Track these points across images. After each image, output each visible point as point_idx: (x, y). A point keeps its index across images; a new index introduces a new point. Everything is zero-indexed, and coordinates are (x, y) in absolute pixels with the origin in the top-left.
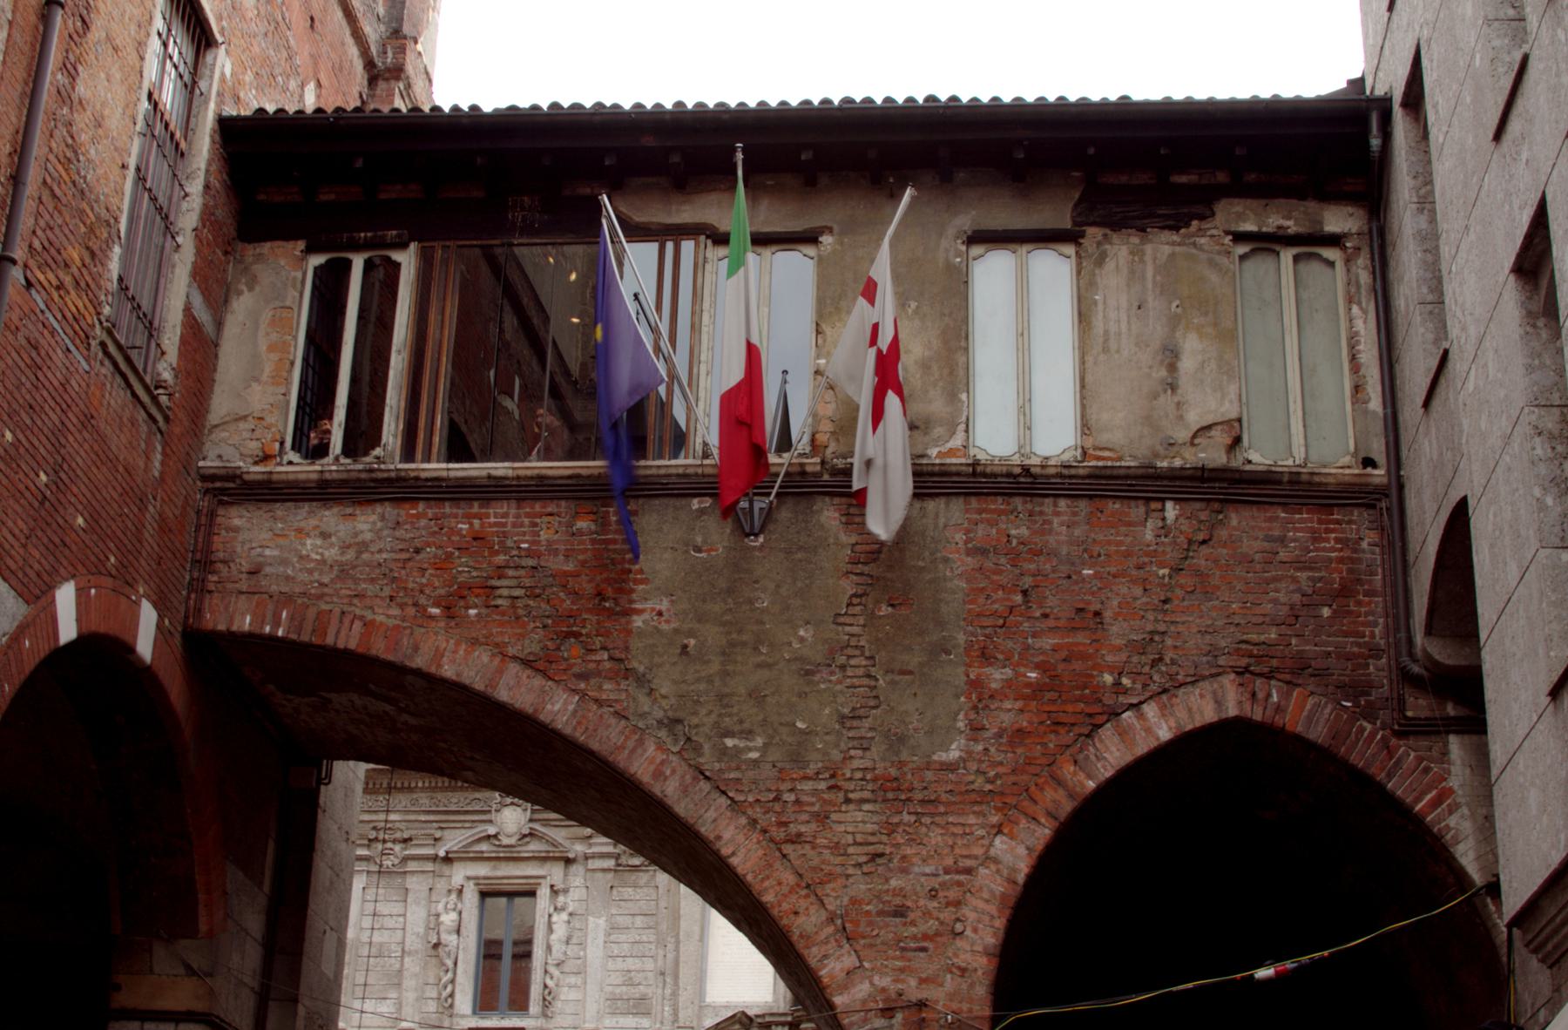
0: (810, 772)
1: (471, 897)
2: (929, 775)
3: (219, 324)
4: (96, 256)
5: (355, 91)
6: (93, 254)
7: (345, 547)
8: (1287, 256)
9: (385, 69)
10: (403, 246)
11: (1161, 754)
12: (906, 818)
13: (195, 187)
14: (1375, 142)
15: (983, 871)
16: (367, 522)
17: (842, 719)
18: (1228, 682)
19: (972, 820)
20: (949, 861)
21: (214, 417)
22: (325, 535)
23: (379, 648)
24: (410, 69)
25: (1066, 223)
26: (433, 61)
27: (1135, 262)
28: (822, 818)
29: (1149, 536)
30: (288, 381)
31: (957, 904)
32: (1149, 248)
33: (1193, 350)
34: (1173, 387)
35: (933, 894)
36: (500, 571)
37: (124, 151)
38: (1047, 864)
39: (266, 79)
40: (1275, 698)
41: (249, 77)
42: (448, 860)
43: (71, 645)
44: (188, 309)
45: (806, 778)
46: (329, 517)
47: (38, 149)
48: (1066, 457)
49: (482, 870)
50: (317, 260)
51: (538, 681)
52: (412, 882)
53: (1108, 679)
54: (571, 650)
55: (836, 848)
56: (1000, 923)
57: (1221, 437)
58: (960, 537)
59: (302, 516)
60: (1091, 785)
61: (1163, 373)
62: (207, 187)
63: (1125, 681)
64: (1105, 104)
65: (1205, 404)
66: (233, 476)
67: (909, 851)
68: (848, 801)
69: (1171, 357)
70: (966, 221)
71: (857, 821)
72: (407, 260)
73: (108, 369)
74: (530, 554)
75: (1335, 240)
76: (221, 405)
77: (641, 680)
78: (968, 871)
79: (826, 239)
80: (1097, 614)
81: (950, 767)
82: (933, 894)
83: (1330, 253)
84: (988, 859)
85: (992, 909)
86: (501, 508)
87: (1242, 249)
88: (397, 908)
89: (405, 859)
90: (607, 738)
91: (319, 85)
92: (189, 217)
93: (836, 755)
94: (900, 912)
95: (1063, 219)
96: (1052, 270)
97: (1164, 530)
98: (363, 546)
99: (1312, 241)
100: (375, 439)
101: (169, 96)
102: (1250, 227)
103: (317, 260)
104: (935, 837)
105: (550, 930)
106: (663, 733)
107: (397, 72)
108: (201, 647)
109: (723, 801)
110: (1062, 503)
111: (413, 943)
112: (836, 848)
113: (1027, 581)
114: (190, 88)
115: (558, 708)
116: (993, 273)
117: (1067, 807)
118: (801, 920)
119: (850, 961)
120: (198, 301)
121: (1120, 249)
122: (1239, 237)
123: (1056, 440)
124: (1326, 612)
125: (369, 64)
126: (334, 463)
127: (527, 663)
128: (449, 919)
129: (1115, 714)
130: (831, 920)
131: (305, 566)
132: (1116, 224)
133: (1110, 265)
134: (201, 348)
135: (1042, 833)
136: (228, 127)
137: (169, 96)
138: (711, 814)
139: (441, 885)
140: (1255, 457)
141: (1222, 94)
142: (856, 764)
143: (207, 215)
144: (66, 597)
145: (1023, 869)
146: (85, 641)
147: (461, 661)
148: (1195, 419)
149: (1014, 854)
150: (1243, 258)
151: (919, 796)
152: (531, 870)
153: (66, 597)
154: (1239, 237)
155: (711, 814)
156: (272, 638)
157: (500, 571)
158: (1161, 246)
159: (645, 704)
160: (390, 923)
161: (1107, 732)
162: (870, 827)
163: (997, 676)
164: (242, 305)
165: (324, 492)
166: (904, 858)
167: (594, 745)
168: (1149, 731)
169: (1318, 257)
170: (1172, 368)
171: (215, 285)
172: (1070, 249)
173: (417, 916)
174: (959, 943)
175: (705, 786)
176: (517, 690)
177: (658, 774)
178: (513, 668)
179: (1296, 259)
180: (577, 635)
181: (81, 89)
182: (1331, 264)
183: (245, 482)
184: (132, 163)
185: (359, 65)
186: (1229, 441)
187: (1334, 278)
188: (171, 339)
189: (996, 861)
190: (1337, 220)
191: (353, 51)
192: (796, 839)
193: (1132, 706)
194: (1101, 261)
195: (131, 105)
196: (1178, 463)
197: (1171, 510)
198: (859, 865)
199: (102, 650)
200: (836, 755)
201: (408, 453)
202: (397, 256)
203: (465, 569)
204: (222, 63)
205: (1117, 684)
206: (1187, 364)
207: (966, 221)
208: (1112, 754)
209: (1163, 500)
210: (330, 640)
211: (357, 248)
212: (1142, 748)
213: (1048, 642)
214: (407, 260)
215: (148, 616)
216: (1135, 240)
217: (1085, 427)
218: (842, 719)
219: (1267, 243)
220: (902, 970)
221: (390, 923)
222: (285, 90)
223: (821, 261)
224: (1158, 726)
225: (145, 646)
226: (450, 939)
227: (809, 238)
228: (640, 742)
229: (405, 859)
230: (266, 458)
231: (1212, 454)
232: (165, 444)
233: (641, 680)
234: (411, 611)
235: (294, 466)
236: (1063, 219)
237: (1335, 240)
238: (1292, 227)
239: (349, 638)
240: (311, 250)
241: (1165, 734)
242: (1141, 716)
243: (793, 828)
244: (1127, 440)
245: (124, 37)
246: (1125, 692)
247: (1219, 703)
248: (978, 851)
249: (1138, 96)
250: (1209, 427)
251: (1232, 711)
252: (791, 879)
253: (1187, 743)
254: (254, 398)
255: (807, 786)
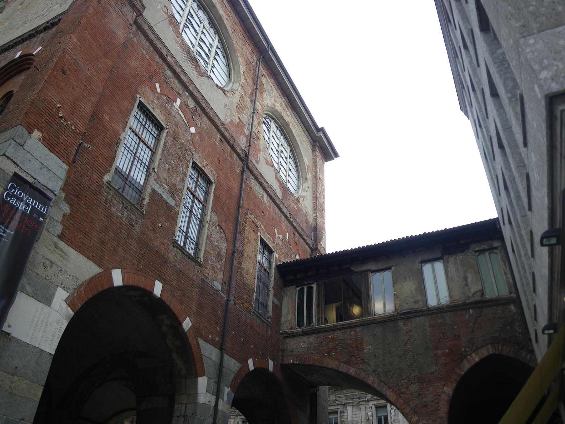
0: (403, 378)
1: (374, 409)
2: (428, 376)
3: (281, 304)
4: (251, 296)
5: (308, 254)
6: (249, 296)
7: (308, 344)
8: (487, 253)
9: (314, 249)
10: (313, 283)
11: (477, 365)
12: (425, 385)
13: (272, 279)
14: (498, 227)
15: (442, 395)
16: (312, 338)
17: (409, 366)
18: (489, 346)
19: (439, 384)
20: (435, 394)
21: (282, 322)
22: (304, 342)
23: (317, 363)
24: (319, 248)
25: (440, 256)
26: (325, 245)
27: (455, 260)
28: (407, 388)
29: (467, 317)
30: (295, 313)
31: (438, 403)
32: (458, 258)
33: (470, 277)
34: (467, 285)
35: (432, 401)
36: (338, 345)
37: (254, 276)
38: (456, 391)
39: (286, 256)
40: (500, 348)
41: (282, 256)
42: (368, 401)
43: (252, 371)
44: (273, 302)
45: (403, 379)
46: (305, 338)
47: (234, 278)
48: (448, 303)
49: (375, 402)
50: (298, 289)
51: (347, 366)
52: (361, 406)
53: (463, 349)
54: (353, 359)
55: (411, 394)
56: (448, 406)
57: (479, 294)
58: (428, 324)
59: (300, 339)
60: (463, 373)
61: (465, 282)
62: (275, 279)
63: (467, 349)
64: (442, 230)
65: (474, 288)
66: (286, 333)
67: (426, 393)
68: (412, 383)
69: (466, 279)
70: (420, 259)
71: (414, 388)
72: (314, 286)
73: (255, 316)
74: (343, 340)
75: (497, 248)
76: (283, 319)
77: (367, 363)
78: (439, 395)
79: (393, 268)
80: (459, 336)
81: (432, 373)
82: (432, 401)
83: (496, 251)
84: (443, 392)
85: (446, 403)
86: (336, 332)
87: (477, 254)
88: (359, 412)
89: (360, 402)
90: (362, 376)
91: (299, 255)
92: (272, 285)
93: (408, 374)
94: (426, 406)
95: (439, 254)
96: (439, 266)
97: (470, 315)
98: (311, 343)
99: (491, 249)
100: (312, 322)
101: (265, 264)
102: (478, 249)
103: (298, 289)
104: (431, 389)
105: (391, 413)
106: (373, 374)
107: (316, 249)
108: (285, 368)
109: (387, 387)
110: (448, 313)
111: (363, 419)
112: (411, 394)
113: (443, 331)
114: (269, 262)
115: (352, 371)
116: (427, 269)
117: (459, 378)
118: (406, 410)
119: (417, 418)
120: (275, 300)
121: (452, 259)
122: (476, 252)
123: (445, 299)
124: (508, 327)
125: (311, 248)
126: (305, 327)
127: (345, 363)
128: (370, 413)
129: (466, 357)
130: (412, 409)
131: (300, 347)
132: (450, 254)
133: (450, 262)
134: (277, 309)
135: (454, 385)
136: (278, 267)
137: (265, 264)
138: (384, 389)
139: (367, 406)
140: (487, 297)
141: (483, 220)
142: (413, 375)
143: (275, 284)
144: (250, 362)
145: (451, 393)
146: (255, 369)
147: (332, 364)
148: (473, 291)
149: (449, 390)
150: (478, 256)
151: (426, 380)
152: (336, 407)
153: (250, 362)
154: (476, 252)
155: (384, 389)
156: (296, 364)
157: (338, 345)
158: (460, 257)
159: (369, 368)
160: (358, 416)
161: (465, 361)
162: (417, 388)
163: (440, 352)
164: (285, 300)
165: (304, 334)
166: (425, 394)
167: (359, 378)
168: (474, 359)
169: (494, 252)
170: (466, 281)
171: (279, 296)
172: (442, 261)
173: (363, 413)
174: (440, 412)
175: (382, 384)
176: (343, 368)
177: (373, 382)
178: (342, 364)
179: (489, 253)
180: (354, 356)
181: (243, 266)
182: (497, 253)
183: (289, 334)
184: (256, 277)
185: (309, 249)
186: (480, 294)
187: (497, 257)
188: (270, 308)
189: (445, 392)
190: (496, 244)
191: (307, 247)
192: (402, 393)
193: (469, 355)
194: (448, 262)
195: (254, 268)
196: (471, 301)
197: (471, 311)
198: (416, 397)
199: (260, 371)
200: (408, 374)
201: (318, 324)
202: (313, 286)
203: (331, 345)
204: (276, 255)
205: (465, 350)
206: (469, 280)
207: (420, 259)
208: (466, 366)
209: (469, 309)
210: (307, 363)
211: (305, 285)
212: (473, 363)
213: (449, 343)
214: (314, 286)
215: (271, 363)
216: (455, 256)
217: (450, 296)
218: (409, 366)
219: (482, 251)
220: (428, 419)
221: (358, 416)
222: (291, 257)
223: (392, 272)
224: (476, 358)
225: (271, 368)
226: (371, 418)
227: (389, 268)
228: (369, 376)
229: (360, 402)
230: (292, 328)
231: (478, 298)
232: (271, 329)
233: (367, 363)
234: (321, 355)
235: (298, 330)
236: (439, 255)
237: (497, 248)
238: (486, 247)
239: (311, 362)
240: (297, 287)
241: (477, 359)
242: (472, 357)
243: (402, 391)
244: (459, 297)
245: (252, 255)
246: (467, 351)
247: (488, 351)
248: (441, 391)
249: (448, 228)
250: (476, 292)
251: (491, 352)
252: (402, 401)
253: (483, 361)
254: (289, 316)
255: (403, 381)
